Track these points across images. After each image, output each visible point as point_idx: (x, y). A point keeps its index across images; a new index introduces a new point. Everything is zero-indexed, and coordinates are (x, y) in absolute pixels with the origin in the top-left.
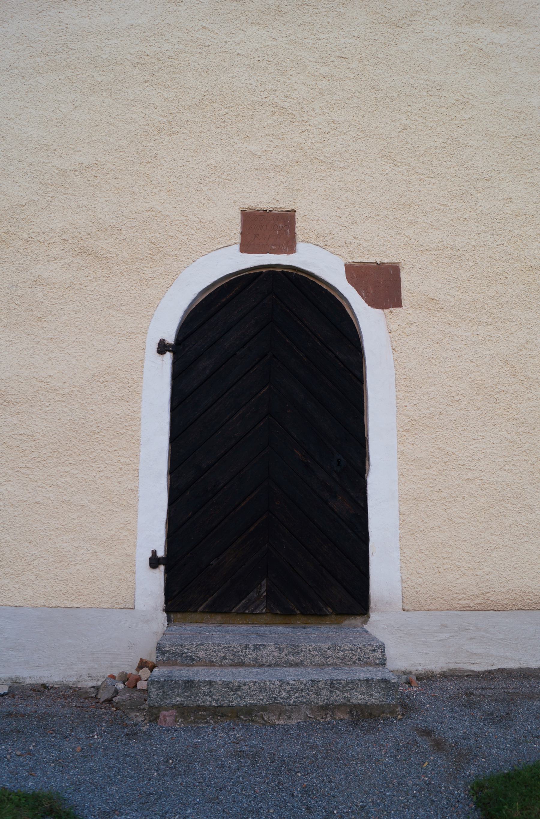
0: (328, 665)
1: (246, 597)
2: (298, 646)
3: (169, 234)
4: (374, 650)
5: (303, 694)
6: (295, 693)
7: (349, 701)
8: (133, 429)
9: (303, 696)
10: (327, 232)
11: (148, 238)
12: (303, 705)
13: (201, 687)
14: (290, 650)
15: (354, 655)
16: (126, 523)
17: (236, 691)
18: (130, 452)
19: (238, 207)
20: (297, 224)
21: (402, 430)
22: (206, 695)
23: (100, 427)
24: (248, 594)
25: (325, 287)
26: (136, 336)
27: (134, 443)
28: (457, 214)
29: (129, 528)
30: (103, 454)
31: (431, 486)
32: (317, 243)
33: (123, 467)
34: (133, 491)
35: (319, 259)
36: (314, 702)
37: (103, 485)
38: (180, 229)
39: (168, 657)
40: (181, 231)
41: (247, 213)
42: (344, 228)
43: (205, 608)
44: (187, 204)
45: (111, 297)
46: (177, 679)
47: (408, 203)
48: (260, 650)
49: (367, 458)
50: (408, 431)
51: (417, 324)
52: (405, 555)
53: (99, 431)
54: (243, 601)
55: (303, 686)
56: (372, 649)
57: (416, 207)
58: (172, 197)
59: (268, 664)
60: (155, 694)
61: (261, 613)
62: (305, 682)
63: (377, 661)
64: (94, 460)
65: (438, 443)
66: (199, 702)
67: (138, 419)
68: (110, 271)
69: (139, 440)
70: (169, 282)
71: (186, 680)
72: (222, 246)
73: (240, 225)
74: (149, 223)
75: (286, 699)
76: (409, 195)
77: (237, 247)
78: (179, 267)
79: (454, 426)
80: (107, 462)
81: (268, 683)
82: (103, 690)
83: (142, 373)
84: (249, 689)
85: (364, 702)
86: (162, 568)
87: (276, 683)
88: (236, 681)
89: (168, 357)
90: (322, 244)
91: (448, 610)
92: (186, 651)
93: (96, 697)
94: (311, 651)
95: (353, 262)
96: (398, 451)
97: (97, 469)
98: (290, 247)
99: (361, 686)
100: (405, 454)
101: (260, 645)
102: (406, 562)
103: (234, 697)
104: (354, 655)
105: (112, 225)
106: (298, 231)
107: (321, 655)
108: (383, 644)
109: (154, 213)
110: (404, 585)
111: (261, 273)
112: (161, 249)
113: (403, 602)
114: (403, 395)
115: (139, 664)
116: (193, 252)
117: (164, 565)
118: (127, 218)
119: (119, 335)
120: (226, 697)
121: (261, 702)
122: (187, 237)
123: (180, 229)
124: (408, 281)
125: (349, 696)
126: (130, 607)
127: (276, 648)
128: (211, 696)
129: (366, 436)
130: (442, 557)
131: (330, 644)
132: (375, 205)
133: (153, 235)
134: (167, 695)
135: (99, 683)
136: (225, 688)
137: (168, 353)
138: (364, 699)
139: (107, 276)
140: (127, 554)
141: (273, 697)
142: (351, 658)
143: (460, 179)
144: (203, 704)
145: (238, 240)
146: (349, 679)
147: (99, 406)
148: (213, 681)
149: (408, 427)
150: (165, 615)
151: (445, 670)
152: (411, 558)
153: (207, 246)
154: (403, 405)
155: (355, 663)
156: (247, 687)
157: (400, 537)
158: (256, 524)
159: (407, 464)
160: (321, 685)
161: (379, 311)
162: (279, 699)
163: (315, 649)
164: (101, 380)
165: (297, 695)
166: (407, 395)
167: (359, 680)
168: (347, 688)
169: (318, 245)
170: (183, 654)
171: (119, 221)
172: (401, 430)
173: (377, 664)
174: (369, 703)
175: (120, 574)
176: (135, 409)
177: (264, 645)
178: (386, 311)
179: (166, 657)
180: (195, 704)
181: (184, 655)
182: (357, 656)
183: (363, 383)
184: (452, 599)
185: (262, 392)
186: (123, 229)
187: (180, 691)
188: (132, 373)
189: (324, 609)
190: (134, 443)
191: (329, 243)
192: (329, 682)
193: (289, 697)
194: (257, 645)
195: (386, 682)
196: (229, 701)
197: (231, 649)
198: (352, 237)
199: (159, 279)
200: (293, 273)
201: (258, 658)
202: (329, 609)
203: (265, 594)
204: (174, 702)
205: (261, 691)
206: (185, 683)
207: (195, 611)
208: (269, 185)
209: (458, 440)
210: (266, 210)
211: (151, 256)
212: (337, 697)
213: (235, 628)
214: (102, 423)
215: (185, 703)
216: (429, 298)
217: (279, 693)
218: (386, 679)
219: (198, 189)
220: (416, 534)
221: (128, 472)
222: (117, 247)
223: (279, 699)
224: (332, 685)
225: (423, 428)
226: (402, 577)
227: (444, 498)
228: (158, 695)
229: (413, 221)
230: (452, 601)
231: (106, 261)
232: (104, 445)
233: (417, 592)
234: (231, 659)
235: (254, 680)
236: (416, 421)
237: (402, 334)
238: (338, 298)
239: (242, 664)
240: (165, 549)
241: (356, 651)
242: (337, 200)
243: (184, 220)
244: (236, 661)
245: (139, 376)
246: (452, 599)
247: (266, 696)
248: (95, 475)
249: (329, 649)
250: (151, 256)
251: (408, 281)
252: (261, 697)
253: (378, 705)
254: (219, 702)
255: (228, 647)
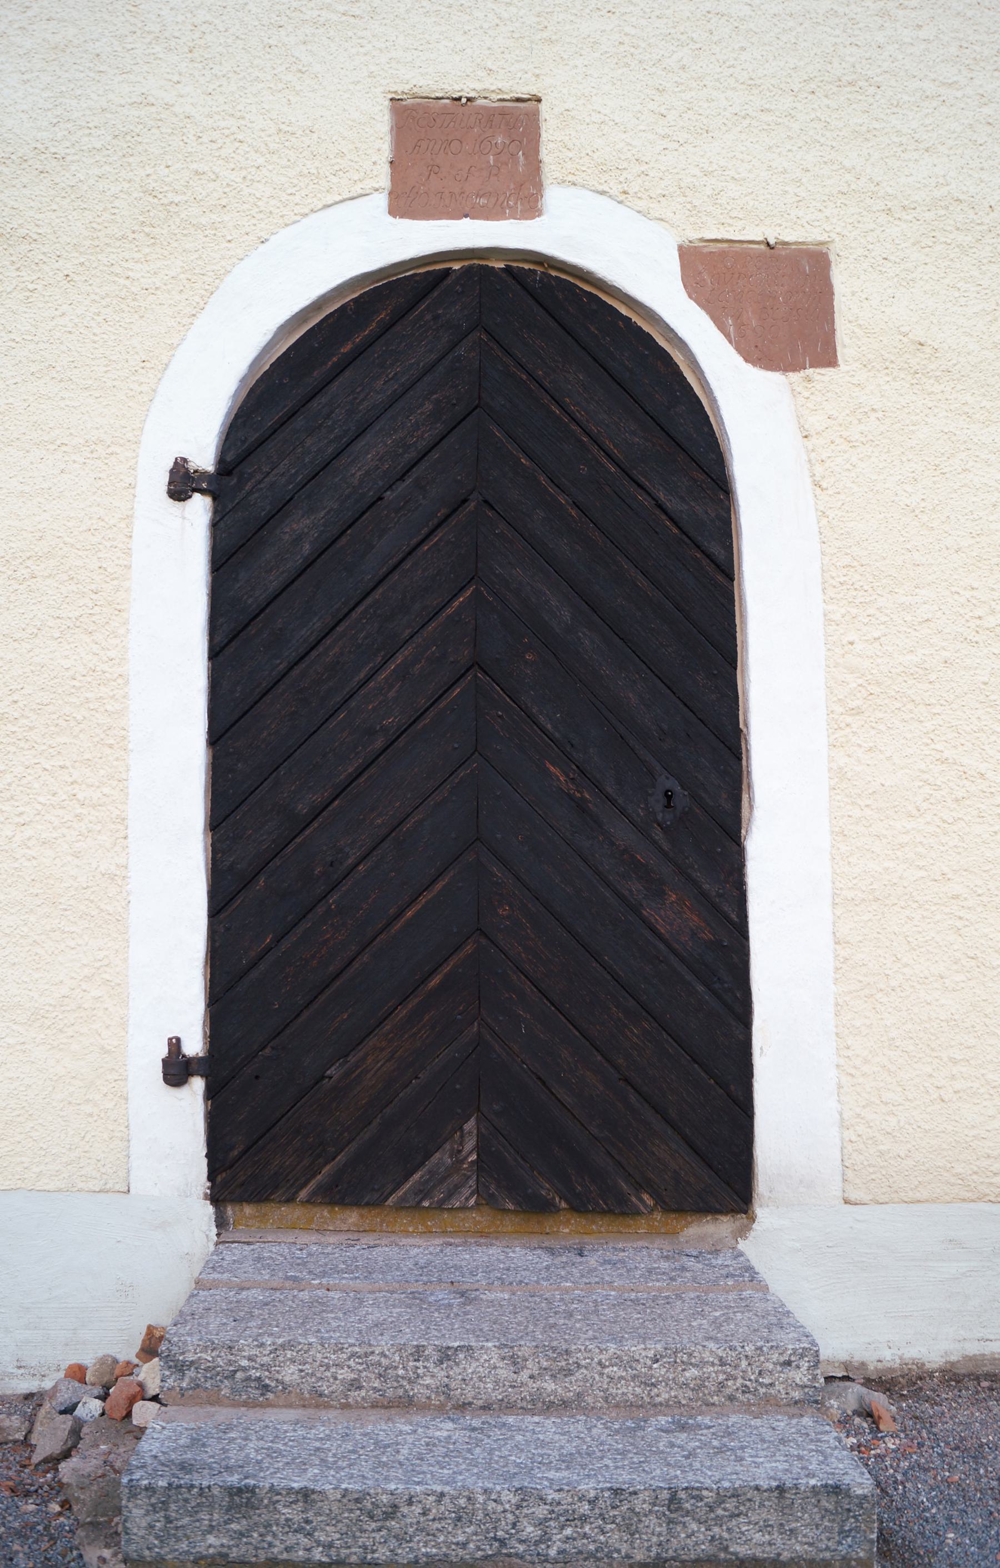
0: (655, 1405)
1: (422, 1164)
2: (567, 1352)
3: (195, 166)
4: (788, 1363)
5: (587, 1529)
6: (562, 1528)
7: (726, 1549)
8: (109, 707)
9: (585, 1536)
10: (629, 155)
11: (138, 179)
12: (585, 1559)
13: (279, 1507)
14: (545, 1364)
15: (730, 1377)
16: (97, 964)
17: (386, 1519)
18: (102, 772)
19: (381, 89)
20: (544, 136)
21: (841, 710)
22: (296, 1531)
23: (21, 704)
24: (428, 1156)
25: (624, 311)
26: (109, 451)
27: (111, 746)
28: (986, 110)
29: (107, 976)
30: (29, 778)
31: (921, 864)
32: (600, 188)
33: (84, 811)
34: (113, 877)
35: (608, 229)
36: (619, 1551)
37: (34, 862)
38: (223, 153)
39: (192, 1380)
40: (226, 159)
41: (406, 108)
42: (676, 145)
43: (314, 1193)
44: (241, 84)
45: (42, 346)
46: (205, 1483)
47: (850, 78)
48: (457, 1364)
49: (744, 787)
50: (856, 711)
51: (880, 415)
52: (850, 1053)
53: (16, 715)
54: (416, 1176)
55: (585, 1508)
56: (782, 1359)
57: (872, 90)
58: (200, 66)
59: (480, 1403)
60: (144, 1524)
61: (463, 1208)
62: (592, 1494)
63: (796, 1395)
64: (8, 794)
65: (938, 747)
66: (275, 1550)
67: (120, 681)
68: (39, 275)
69: (124, 738)
70: (197, 299)
71: (231, 1488)
72: (338, 198)
73: (388, 138)
74: (139, 139)
75: (537, 1543)
76: (851, 55)
77: (382, 201)
78: (223, 258)
79: (982, 698)
80: (41, 799)
81: (481, 1499)
82: (42, 1425)
83: (128, 552)
84: (424, 1514)
85: (770, 1553)
86: (198, 1084)
87: (503, 1498)
88: (385, 1491)
89: (200, 508)
90: (615, 190)
91: (964, 1200)
92: (244, 1363)
93: (26, 1442)
94: (604, 1367)
95: (702, 240)
96: (830, 769)
97: (17, 820)
98: (525, 198)
99: (762, 1505)
100: (849, 775)
101: (456, 1350)
102: (853, 1071)
103: (377, 1536)
104: (730, 1377)
105: (39, 146)
106: (548, 153)
107: (634, 1378)
108: (814, 1343)
109: (153, 109)
110: (846, 1133)
111: (448, 272)
112: (173, 209)
113: (845, 1180)
114: (843, 611)
115: (144, 1341)
116: (261, 216)
117: (202, 1076)
118: (81, 128)
119: (64, 448)
120: (354, 1536)
121: (461, 1552)
122: (244, 173)
123: (223, 153)
124: (853, 294)
125: (726, 1535)
126: (117, 1187)
127: (503, 1359)
128: (309, 1534)
129: (741, 726)
130: (950, 1059)
131: (659, 1347)
132: (758, 82)
133: (149, 171)
134: (177, 1528)
135: (48, 1384)
136: (351, 1511)
137: (197, 496)
138: (770, 1544)
139: (31, 287)
140: (103, 1048)
141: (495, 1539)
142: (722, 1385)
143: (991, 13)
144: (285, 1556)
145: (384, 180)
146: (726, 1484)
147: (16, 645)
148: (313, 1492)
149: (859, 703)
150: (210, 1209)
151: (953, 1358)
152: (866, 1061)
153: (297, 199)
154: (845, 642)
155: (731, 1398)
156: (417, 1509)
157: (837, 1005)
158: (446, 969)
159: (853, 803)
160: (641, 1504)
161: (775, 378)
162: (513, 1542)
163: (617, 1360)
164: (19, 574)
165: (568, 1531)
166: (854, 611)
167: (757, 1488)
168: (720, 1512)
169: (603, 193)
170: (235, 1372)
171: (60, 135)
172: (838, 709)
173: (796, 1403)
174: (786, 1556)
175: (88, 1101)
176: (112, 654)
177: (469, 1348)
178: (794, 377)
179: (187, 1380)
180: (262, 1556)
181: (239, 1375)
182: (740, 1381)
183: (732, 580)
184: (976, 1173)
185: (456, 603)
186: (69, 158)
187: (216, 1516)
188: (100, 555)
189: (634, 1199)
190: (111, 746)
191: (634, 187)
192: (665, 1495)
193: (545, 1539)
194: (449, 1348)
195: (837, 1494)
196: (365, 1548)
197: (375, 1358)
198: (696, 171)
199: (169, 292)
200: (534, 272)
201: (453, 1385)
202: (646, 1197)
203: (474, 1157)
204: (201, 1548)
205: (459, 1519)
206: (231, 1495)
207: (290, 1200)
208: (466, 28)
209: (994, 738)
210: (459, 99)
211: (147, 230)
212: (689, 1537)
213: (392, 1252)
214: (23, 692)
215: (234, 1554)
216: (913, 342)
217: (514, 1525)
218: (837, 1487)
219: (271, 42)
220: (880, 995)
221: (98, 827)
222: (55, 207)
223: (513, 1542)
224: (673, 1503)
225: (898, 705)
226: (841, 1114)
227: (956, 897)
228: (151, 1527)
229: (864, 129)
230: (975, 1177)
231: (25, 247)
232: (33, 752)
233: (881, 1154)
234: (374, 1388)
235: (439, 1488)
236: (878, 684)
237: (838, 441)
238: (662, 342)
239: (406, 1404)
240: (205, 1033)
241: (736, 1367)
242: (654, 69)
243: (234, 129)
244: (390, 1393)
245: (121, 562)
246: (976, 1173)
247: (476, 1534)
248: (10, 834)
249: (657, 1361)
250: (147, 230)
251: (853, 294)
252: (461, 1538)
253: (811, 1562)
254: (333, 1552)
255: (366, 1355)
